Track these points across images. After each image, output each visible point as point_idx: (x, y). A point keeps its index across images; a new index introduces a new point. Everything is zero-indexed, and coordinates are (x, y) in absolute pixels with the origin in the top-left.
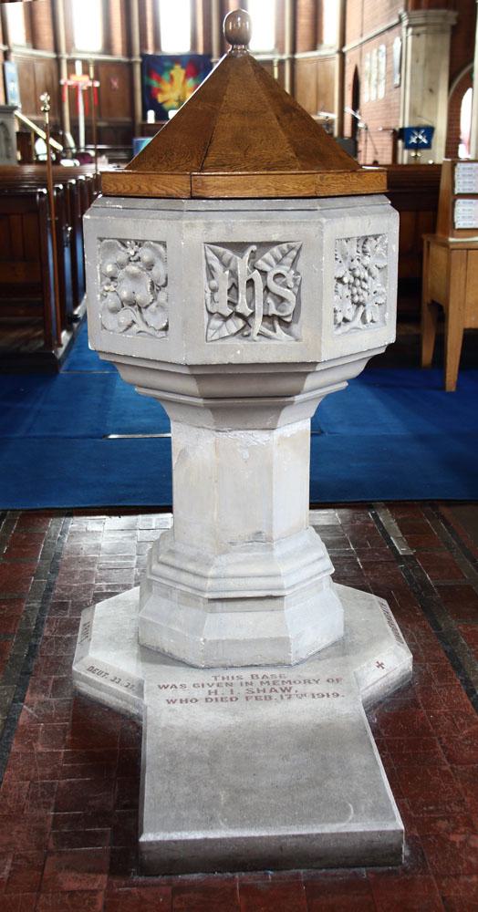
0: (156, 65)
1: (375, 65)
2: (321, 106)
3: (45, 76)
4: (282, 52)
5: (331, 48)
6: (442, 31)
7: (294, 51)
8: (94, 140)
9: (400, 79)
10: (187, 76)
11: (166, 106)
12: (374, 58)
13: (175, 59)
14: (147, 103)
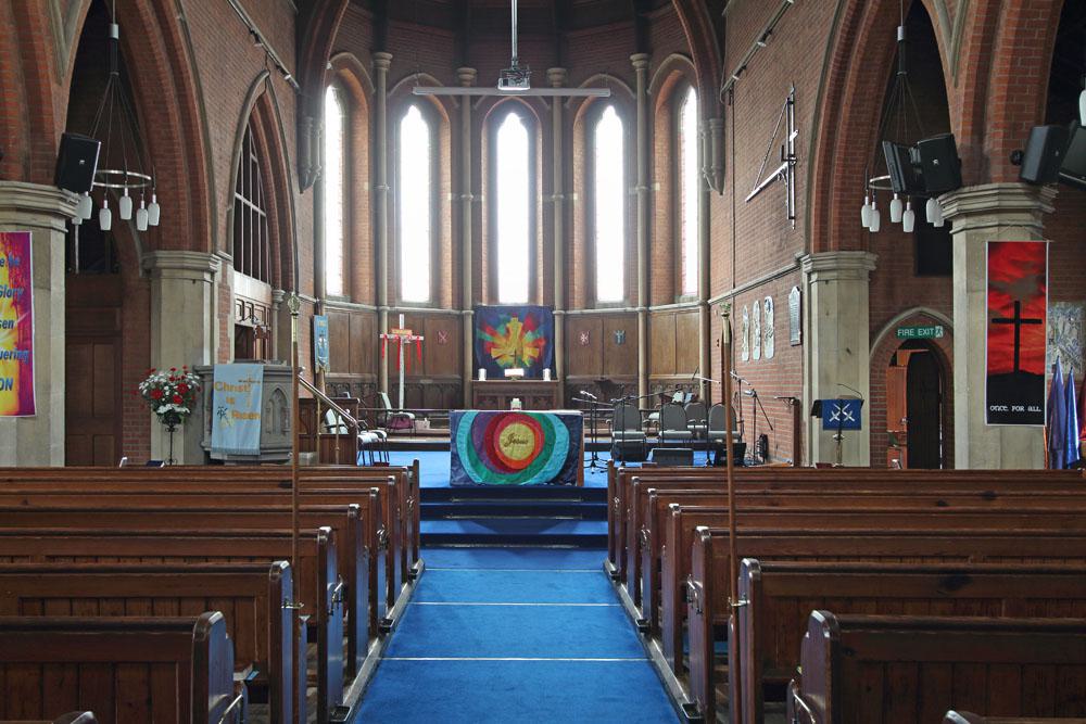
0: (491, 317)
1: (756, 316)
2: (682, 364)
3: (363, 331)
4: (635, 304)
5: (692, 300)
6: (860, 278)
7: (648, 303)
8: (562, 404)
9: (802, 336)
10: (524, 330)
11: (500, 362)
12: (756, 310)
13: (513, 311)
14: (479, 358)
